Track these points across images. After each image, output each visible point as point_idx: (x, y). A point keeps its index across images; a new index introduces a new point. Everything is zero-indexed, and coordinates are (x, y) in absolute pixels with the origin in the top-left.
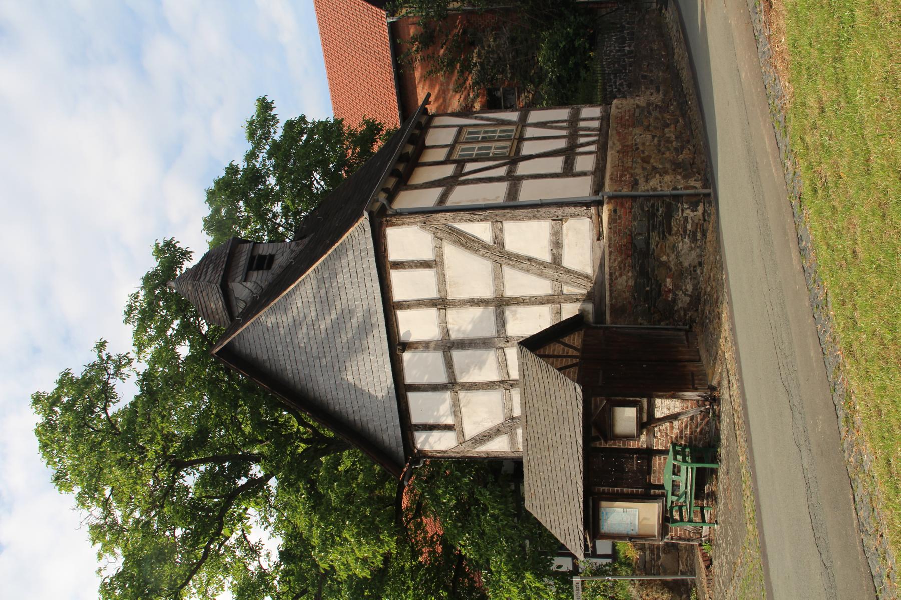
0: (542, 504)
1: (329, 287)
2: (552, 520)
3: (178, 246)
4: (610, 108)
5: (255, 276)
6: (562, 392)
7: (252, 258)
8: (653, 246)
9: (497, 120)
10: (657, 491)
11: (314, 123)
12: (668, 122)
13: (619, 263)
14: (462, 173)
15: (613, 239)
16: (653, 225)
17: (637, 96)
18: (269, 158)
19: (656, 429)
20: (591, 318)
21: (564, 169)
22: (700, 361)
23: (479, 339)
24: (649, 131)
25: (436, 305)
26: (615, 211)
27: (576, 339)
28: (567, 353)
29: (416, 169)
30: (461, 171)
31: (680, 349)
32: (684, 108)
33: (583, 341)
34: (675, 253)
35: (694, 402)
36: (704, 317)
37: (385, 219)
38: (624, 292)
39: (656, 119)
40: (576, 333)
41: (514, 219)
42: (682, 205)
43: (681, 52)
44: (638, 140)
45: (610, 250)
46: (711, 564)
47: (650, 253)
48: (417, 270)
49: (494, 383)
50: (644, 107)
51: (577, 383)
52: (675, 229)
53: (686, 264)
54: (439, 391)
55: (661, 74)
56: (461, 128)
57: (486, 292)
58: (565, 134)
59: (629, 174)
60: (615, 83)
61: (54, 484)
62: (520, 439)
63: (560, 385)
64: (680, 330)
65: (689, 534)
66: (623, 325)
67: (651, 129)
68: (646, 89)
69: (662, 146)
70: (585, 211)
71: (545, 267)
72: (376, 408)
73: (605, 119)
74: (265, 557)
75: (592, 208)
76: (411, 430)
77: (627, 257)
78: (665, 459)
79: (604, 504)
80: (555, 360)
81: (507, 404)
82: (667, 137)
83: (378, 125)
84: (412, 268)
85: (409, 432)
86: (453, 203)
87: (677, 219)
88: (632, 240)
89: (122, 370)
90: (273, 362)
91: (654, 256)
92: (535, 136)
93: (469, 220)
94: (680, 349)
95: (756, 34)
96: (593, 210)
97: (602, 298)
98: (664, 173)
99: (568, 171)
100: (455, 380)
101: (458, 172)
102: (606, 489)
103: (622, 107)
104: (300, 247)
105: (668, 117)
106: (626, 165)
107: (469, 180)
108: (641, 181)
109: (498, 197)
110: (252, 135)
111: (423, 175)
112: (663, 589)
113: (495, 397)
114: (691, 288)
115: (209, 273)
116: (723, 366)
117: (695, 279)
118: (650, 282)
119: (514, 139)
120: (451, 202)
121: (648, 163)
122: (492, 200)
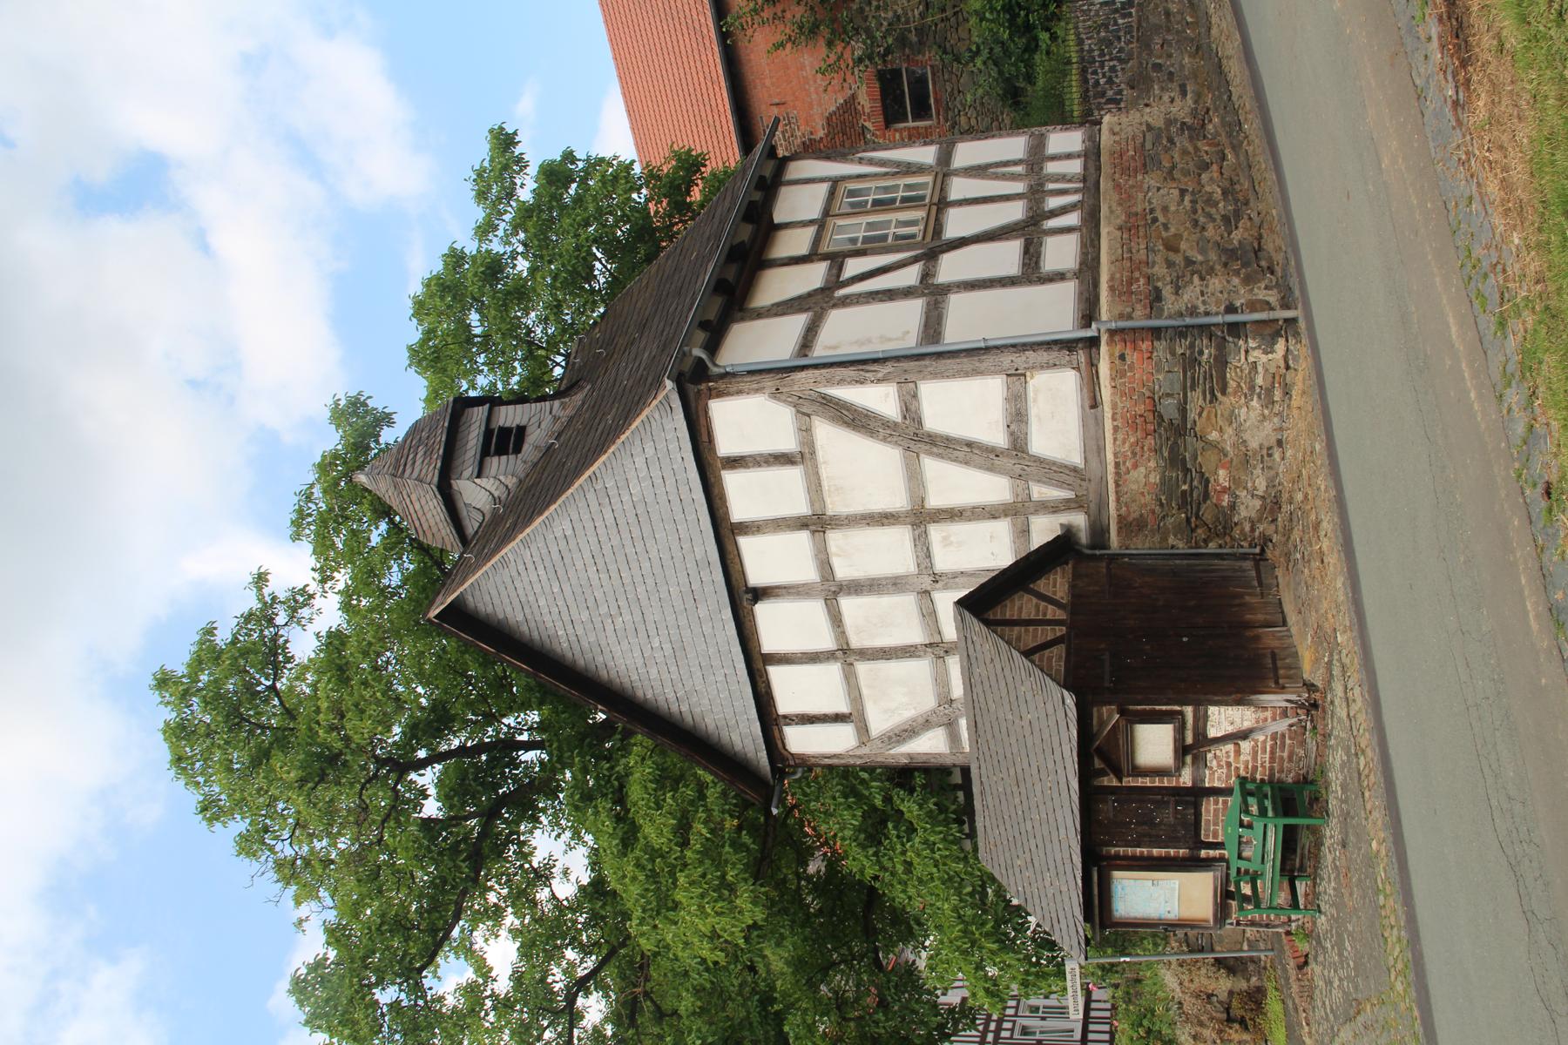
0: (1009, 862)
3: (371, 403)
4: (1100, 130)
5: (494, 464)
6: (1039, 698)
7: (488, 433)
8: (1192, 415)
9: (898, 164)
11: (588, 160)
13: (1131, 446)
14: (841, 279)
15: (1120, 405)
16: (1193, 378)
17: (1147, 105)
19: (1209, 756)
20: (1084, 538)
21: (1024, 265)
22: (1284, 623)
23: (886, 578)
24: (1173, 179)
26: (1122, 357)
27: (1057, 584)
28: (1045, 614)
30: (839, 276)
32: (1235, 134)
33: (1072, 587)
34: (1234, 425)
38: (1143, 493)
39: (1184, 152)
40: (1058, 569)
42: (1246, 342)
43: (1224, 25)
44: (1154, 201)
45: (1115, 423)
46: (1306, 963)
47: (1189, 427)
50: (1159, 128)
52: (1232, 384)
53: (1254, 444)
54: (821, 662)
55: (1186, 60)
56: (835, 182)
57: (898, 501)
59: (1144, 277)
61: (201, 816)
62: (964, 734)
63: (1034, 687)
66: (1142, 545)
67: (1177, 174)
69: (1200, 211)
70: (1067, 358)
71: (997, 456)
72: (716, 692)
73: (1092, 154)
74: (561, 876)
75: (1081, 352)
76: (777, 725)
77: (1147, 435)
78: (1225, 803)
79: (1117, 874)
80: (1023, 629)
81: (941, 681)
84: (760, 466)
85: (775, 728)
87: (1237, 367)
88: (1155, 406)
89: (300, 611)
90: (532, 625)
92: (968, 196)
93: (857, 382)
95: (1418, 82)
96: (1081, 356)
97: (1102, 504)
99: (1032, 272)
100: (848, 644)
101: (834, 279)
102: (1121, 849)
103: (1121, 130)
104: (569, 412)
105: (1206, 148)
108: (1167, 292)
109: (908, 332)
110: (482, 195)
111: (777, 285)
113: (919, 670)
115: (419, 462)
116: (1331, 655)
117: (1270, 468)
118: (1189, 476)
120: (820, 351)
121: (1176, 250)
122: (897, 339)
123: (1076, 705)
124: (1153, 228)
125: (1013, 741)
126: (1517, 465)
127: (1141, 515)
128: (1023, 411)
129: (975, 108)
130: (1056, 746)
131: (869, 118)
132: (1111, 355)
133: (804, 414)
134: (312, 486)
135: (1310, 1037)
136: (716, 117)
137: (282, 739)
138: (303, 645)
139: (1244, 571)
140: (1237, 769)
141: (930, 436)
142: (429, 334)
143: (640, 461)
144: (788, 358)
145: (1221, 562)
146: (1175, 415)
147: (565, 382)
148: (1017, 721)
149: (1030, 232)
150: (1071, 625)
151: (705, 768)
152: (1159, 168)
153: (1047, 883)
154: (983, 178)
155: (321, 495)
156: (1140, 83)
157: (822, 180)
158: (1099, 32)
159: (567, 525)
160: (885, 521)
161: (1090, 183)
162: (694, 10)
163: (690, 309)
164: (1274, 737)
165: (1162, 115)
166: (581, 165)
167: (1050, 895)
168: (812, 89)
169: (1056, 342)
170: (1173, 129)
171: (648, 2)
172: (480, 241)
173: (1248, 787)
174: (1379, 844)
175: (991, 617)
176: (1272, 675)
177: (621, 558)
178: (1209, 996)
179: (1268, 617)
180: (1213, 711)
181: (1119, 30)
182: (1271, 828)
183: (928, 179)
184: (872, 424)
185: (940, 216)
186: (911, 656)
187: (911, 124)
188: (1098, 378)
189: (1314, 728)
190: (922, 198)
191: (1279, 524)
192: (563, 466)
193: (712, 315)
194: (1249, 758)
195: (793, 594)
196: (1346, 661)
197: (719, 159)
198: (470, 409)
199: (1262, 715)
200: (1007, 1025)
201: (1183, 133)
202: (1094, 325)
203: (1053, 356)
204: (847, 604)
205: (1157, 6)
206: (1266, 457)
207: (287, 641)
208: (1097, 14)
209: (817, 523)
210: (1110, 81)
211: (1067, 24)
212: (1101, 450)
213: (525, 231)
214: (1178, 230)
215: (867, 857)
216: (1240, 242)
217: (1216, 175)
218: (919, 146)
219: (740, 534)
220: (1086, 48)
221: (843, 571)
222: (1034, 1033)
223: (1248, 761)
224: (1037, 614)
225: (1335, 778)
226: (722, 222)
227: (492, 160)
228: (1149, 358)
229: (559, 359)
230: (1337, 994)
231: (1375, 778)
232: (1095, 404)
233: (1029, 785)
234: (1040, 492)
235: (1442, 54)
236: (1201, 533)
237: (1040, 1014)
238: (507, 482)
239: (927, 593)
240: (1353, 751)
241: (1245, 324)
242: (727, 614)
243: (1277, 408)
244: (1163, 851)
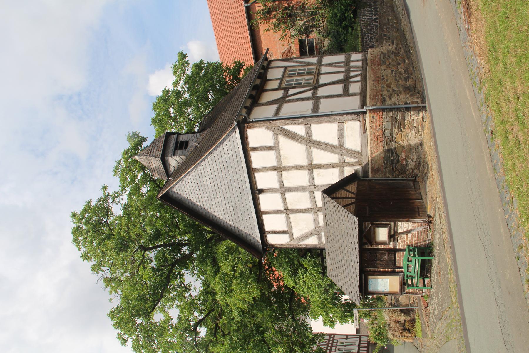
0: (336, 275)
2: (342, 284)
4: (367, 54)
6: (347, 220)
7: (177, 143)
8: (394, 136)
9: (305, 63)
10: (399, 270)
11: (208, 63)
15: (372, 132)
17: (382, 46)
18: (185, 84)
20: (361, 174)
22: (422, 199)
23: (300, 187)
24: (389, 67)
25: (276, 169)
27: (353, 187)
28: (349, 196)
30: (287, 94)
31: (411, 192)
33: (357, 188)
35: (420, 224)
36: (424, 175)
37: (246, 125)
38: (379, 160)
39: (393, 60)
40: (353, 183)
42: (411, 113)
43: (405, 22)
44: (384, 73)
46: (428, 306)
47: (393, 139)
48: (265, 151)
49: (308, 209)
55: (394, 33)
56: (286, 68)
57: (303, 161)
58: (343, 70)
60: (368, 36)
62: (323, 238)
65: (416, 291)
66: (378, 177)
68: (386, 42)
69: (397, 76)
71: (335, 148)
73: (365, 60)
75: (361, 116)
77: (381, 142)
78: (403, 254)
79: (370, 277)
80: (342, 200)
81: (316, 221)
82: (400, 71)
83: (242, 63)
86: (283, 114)
87: (408, 121)
89: (116, 199)
91: (395, 141)
93: (292, 124)
94: (411, 192)
95: (458, 26)
96: (361, 117)
98: (399, 94)
99: (346, 93)
100: (287, 208)
101: (285, 95)
102: (371, 269)
103: (374, 53)
106: (378, 89)
107: (291, 99)
108: (387, 99)
110: (175, 72)
111: (267, 97)
112: (401, 313)
113: (310, 216)
114: (416, 157)
116: (435, 206)
117: (418, 152)
118: (393, 155)
119: (315, 74)
120: (282, 114)
121: (390, 87)
122: (305, 112)
123: (358, 221)
125: (338, 234)
126: (484, 128)
127: (379, 167)
128: (343, 134)
129: (329, 52)
130: (352, 234)
131: (295, 54)
132: (370, 117)
133: (276, 134)
134: (121, 160)
135: (429, 331)
136: (247, 53)
137: (109, 237)
138: (117, 210)
139: (410, 184)
140: (407, 242)
141: (314, 141)
142: (158, 114)
143: (225, 148)
144: (272, 116)
145: (402, 182)
146: (389, 135)
148: (340, 228)
149: (346, 82)
150: (357, 199)
151: (242, 247)
152: (385, 64)
153: (348, 280)
154: (331, 67)
155: (123, 163)
156: (380, 41)
157: (282, 67)
158: (367, 27)
159: (202, 169)
160: (300, 168)
161: (364, 68)
162: (241, 20)
163: (241, 103)
164: (418, 232)
166: (206, 65)
167: (349, 284)
168: (278, 45)
169: (353, 113)
170: (390, 53)
172: (174, 87)
173: (412, 249)
174: (449, 259)
175: (332, 196)
176: (417, 213)
177: (218, 180)
178: (398, 322)
179: (417, 197)
180: (400, 224)
181: (373, 26)
183: (314, 67)
184: (297, 138)
185: (318, 77)
188: (366, 124)
189: (430, 229)
190: (313, 72)
191: (420, 170)
192: (201, 151)
195: (270, 191)
196: (439, 206)
197: (249, 63)
199: (414, 225)
200: (333, 348)
202: (365, 108)
204: (288, 195)
205: (385, 18)
206: (416, 149)
207: (111, 208)
208: (367, 22)
209: (279, 169)
210: (371, 41)
211: (357, 24)
212: (366, 146)
213: (189, 84)
214: (390, 81)
215: (291, 279)
216: (409, 85)
217: (402, 66)
219: (255, 172)
220: (363, 31)
221: (287, 184)
222: (342, 351)
224: (346, 196)
225: (436, 244)
226: (251, 79)
227: (179, 62)
228: (381, 118)
229: (197, 124)
230: (437, 312)
231: (448, 239)
232: (365, 132)
233: (343, 248)
234: (348, 159)
235: (464, 16)
236: (397, 173)
237: (344, 345)
238: (182, 158)
240: (441, 233)
241: (410, 108)
242: (250, 197)
244: (384, 269)
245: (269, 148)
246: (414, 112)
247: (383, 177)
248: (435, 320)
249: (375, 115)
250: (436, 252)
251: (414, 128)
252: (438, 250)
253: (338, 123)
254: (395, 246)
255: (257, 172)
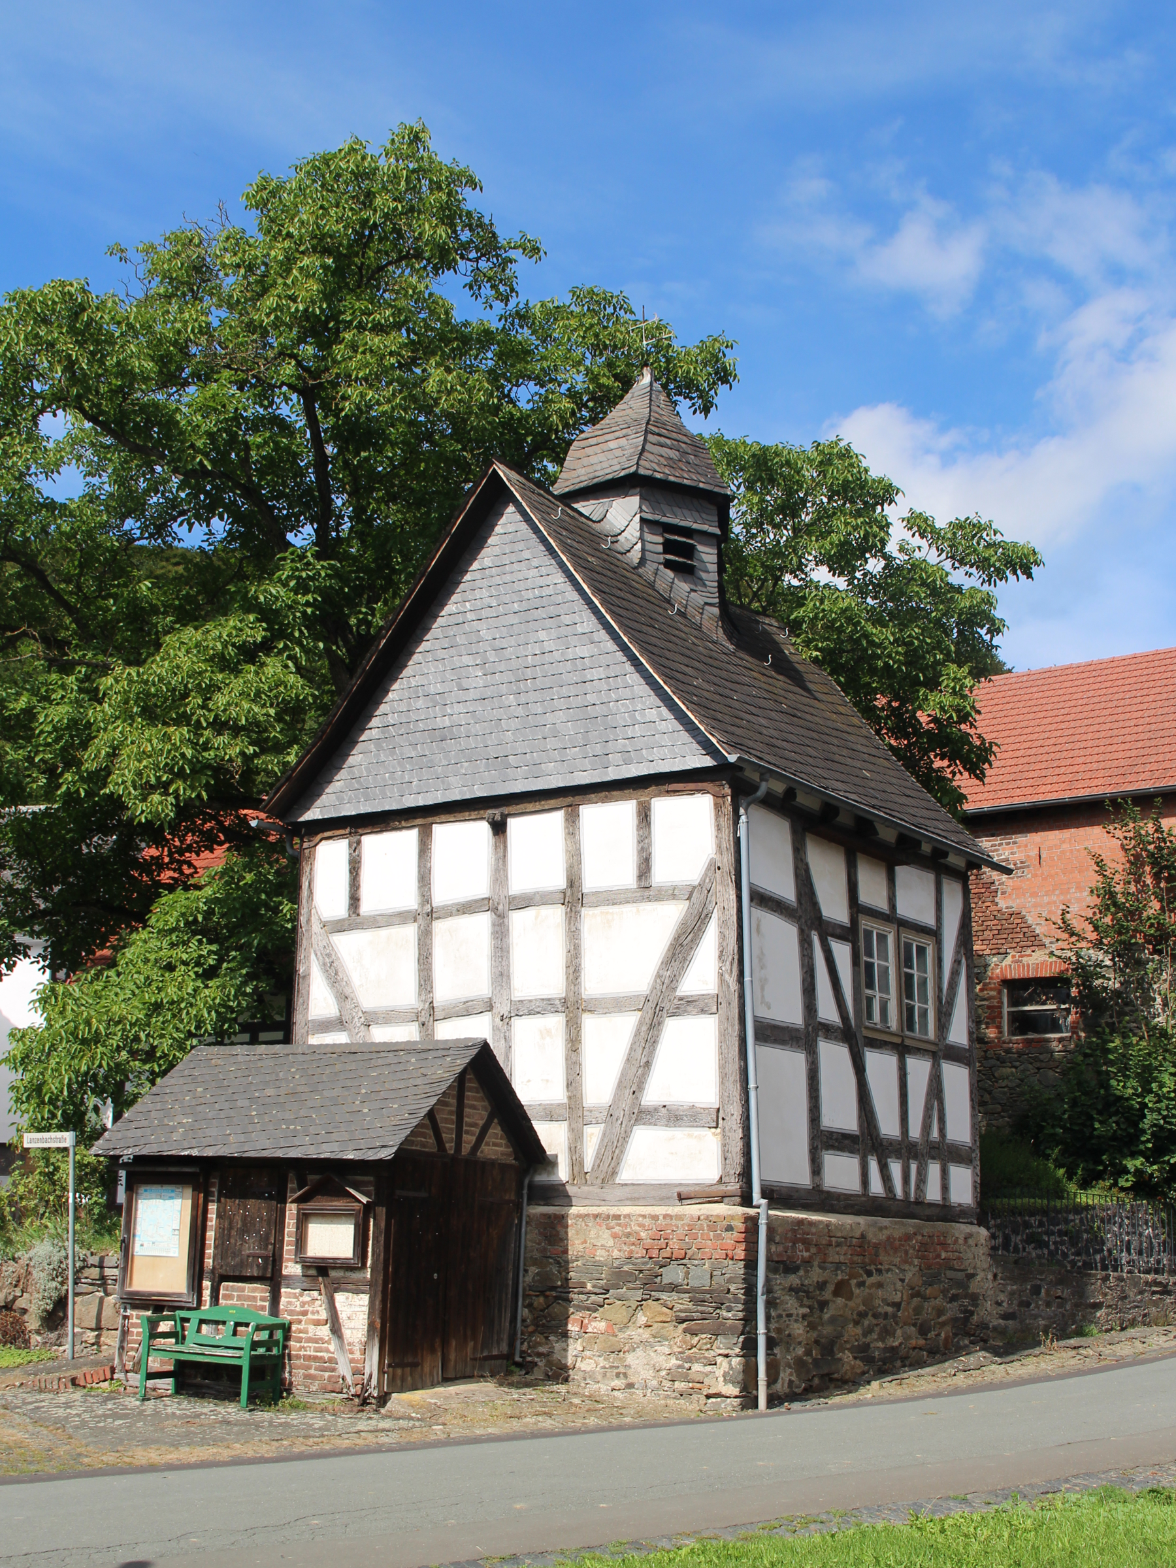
1: (358, 783)
4: (972, 1223)
7: (688, 532)
8: (664, 1296)
9: (951, 1002)
12: (932, 1335)
14: (829, 938)
15: (680, 1223)
17: (995, 1276)
19: (315, 1294)
20: (541, 1178)
21: (832, 1133)
23: (508, 966)
24: (913, 1296)
26: (729, 1228)
27: (496, 1147)
28: (467, 1132)
29: (842, 849)
30: (833, 936)
31: (471, 1344)
33: (493, 1163)
37: (727, 790)
39: (940, 1312)
41: (723, 1035)
42: (738, 1356)
44: (889, 1275)
51: (399, 1149)
56: (935, 934)
57: (592, 986)
58: (911, 1134)
59: (810, 1257)
64: (512, 1345)
65: (132, 1349)
66: (530, 1238)
67: (916, 1301)
73: (946, 1212)
75: (738, 1186)
76: (350, 833)
78: (263, 1308)
80: (454, 1109)
81: (390, 1017)
86: (759, 921)
88: (677, 1259)
92: (909, 1078)
93: (722, 952)
94: (471, 1344)
96: (734, 1187)
101: (830, 930)
103: (969, 1246)
105: (943, 1335)
106: (831, 1251)
108: (793, 1280)
109: (769, 1008)
113: (407, 995)
116: (418, 1419)
117: (605, 1375)
121: (837, 1293)
122: (763, 996)
123: (381, 1160)
124: (861, 1271)
128: (680, 1122)
129: (1018, 1086)
132: (732, 1217)
139: (498, 1343)
140: (300, 1322)
145: (508, 1319)
147: (738, 611)
150: (455, 1159)
152: (925, 1283)
154: (928, 1094)
157: (939, 919)
158: (1086, 1231)
160: (571, 970)
161: (914, 1208)
164: (332, 1360)
165: (982, 1291)
168: (1054, 898)
171: (1173, 709)
179: (452, 1363)
181: (1088, 1254)
182: (237, 1353)
183: (931, 1034)
184: (675, 964)
186: (420, 985)
187: (1006, 1009)
190: (911, 1027)
193: (802, 799)
194: (310, 1335)
195: (498, 860)
198: (716, 512)
199: (357, 1349)
201: (961, 1312)
202: (764, 1201)
203: (737, 1159)
204: (483, 921)
212: (634, 1200)
216: (840, 1359)
217: (913, 1342)
218: (969, 1027)
219: (567, 813)
220: (1071, 1217)
221: (518, 920)
223: (307, 1332)
230: (61, 1412)
232: (681, 1198)
234: (593, 1136)
239: (489, 1006)
242: (480, 792)
243: (668, 1384)
245: (645, 867)
246: (740, 1368)
247: (528, 1255)
248: (32, 1407)
249: (736, 1234)
250: (263, 1415)
251: (687, 1365)
252: (271, 1423)
253: (718, 1110)
254: (290, 1281)
255: (567, 820)
